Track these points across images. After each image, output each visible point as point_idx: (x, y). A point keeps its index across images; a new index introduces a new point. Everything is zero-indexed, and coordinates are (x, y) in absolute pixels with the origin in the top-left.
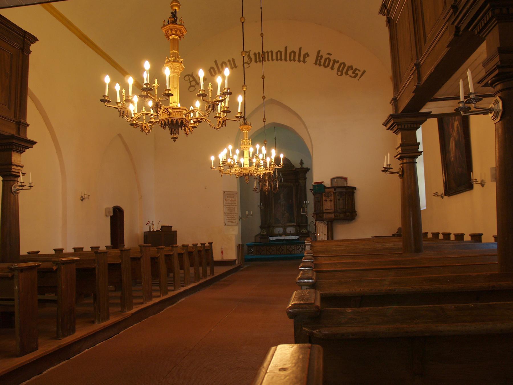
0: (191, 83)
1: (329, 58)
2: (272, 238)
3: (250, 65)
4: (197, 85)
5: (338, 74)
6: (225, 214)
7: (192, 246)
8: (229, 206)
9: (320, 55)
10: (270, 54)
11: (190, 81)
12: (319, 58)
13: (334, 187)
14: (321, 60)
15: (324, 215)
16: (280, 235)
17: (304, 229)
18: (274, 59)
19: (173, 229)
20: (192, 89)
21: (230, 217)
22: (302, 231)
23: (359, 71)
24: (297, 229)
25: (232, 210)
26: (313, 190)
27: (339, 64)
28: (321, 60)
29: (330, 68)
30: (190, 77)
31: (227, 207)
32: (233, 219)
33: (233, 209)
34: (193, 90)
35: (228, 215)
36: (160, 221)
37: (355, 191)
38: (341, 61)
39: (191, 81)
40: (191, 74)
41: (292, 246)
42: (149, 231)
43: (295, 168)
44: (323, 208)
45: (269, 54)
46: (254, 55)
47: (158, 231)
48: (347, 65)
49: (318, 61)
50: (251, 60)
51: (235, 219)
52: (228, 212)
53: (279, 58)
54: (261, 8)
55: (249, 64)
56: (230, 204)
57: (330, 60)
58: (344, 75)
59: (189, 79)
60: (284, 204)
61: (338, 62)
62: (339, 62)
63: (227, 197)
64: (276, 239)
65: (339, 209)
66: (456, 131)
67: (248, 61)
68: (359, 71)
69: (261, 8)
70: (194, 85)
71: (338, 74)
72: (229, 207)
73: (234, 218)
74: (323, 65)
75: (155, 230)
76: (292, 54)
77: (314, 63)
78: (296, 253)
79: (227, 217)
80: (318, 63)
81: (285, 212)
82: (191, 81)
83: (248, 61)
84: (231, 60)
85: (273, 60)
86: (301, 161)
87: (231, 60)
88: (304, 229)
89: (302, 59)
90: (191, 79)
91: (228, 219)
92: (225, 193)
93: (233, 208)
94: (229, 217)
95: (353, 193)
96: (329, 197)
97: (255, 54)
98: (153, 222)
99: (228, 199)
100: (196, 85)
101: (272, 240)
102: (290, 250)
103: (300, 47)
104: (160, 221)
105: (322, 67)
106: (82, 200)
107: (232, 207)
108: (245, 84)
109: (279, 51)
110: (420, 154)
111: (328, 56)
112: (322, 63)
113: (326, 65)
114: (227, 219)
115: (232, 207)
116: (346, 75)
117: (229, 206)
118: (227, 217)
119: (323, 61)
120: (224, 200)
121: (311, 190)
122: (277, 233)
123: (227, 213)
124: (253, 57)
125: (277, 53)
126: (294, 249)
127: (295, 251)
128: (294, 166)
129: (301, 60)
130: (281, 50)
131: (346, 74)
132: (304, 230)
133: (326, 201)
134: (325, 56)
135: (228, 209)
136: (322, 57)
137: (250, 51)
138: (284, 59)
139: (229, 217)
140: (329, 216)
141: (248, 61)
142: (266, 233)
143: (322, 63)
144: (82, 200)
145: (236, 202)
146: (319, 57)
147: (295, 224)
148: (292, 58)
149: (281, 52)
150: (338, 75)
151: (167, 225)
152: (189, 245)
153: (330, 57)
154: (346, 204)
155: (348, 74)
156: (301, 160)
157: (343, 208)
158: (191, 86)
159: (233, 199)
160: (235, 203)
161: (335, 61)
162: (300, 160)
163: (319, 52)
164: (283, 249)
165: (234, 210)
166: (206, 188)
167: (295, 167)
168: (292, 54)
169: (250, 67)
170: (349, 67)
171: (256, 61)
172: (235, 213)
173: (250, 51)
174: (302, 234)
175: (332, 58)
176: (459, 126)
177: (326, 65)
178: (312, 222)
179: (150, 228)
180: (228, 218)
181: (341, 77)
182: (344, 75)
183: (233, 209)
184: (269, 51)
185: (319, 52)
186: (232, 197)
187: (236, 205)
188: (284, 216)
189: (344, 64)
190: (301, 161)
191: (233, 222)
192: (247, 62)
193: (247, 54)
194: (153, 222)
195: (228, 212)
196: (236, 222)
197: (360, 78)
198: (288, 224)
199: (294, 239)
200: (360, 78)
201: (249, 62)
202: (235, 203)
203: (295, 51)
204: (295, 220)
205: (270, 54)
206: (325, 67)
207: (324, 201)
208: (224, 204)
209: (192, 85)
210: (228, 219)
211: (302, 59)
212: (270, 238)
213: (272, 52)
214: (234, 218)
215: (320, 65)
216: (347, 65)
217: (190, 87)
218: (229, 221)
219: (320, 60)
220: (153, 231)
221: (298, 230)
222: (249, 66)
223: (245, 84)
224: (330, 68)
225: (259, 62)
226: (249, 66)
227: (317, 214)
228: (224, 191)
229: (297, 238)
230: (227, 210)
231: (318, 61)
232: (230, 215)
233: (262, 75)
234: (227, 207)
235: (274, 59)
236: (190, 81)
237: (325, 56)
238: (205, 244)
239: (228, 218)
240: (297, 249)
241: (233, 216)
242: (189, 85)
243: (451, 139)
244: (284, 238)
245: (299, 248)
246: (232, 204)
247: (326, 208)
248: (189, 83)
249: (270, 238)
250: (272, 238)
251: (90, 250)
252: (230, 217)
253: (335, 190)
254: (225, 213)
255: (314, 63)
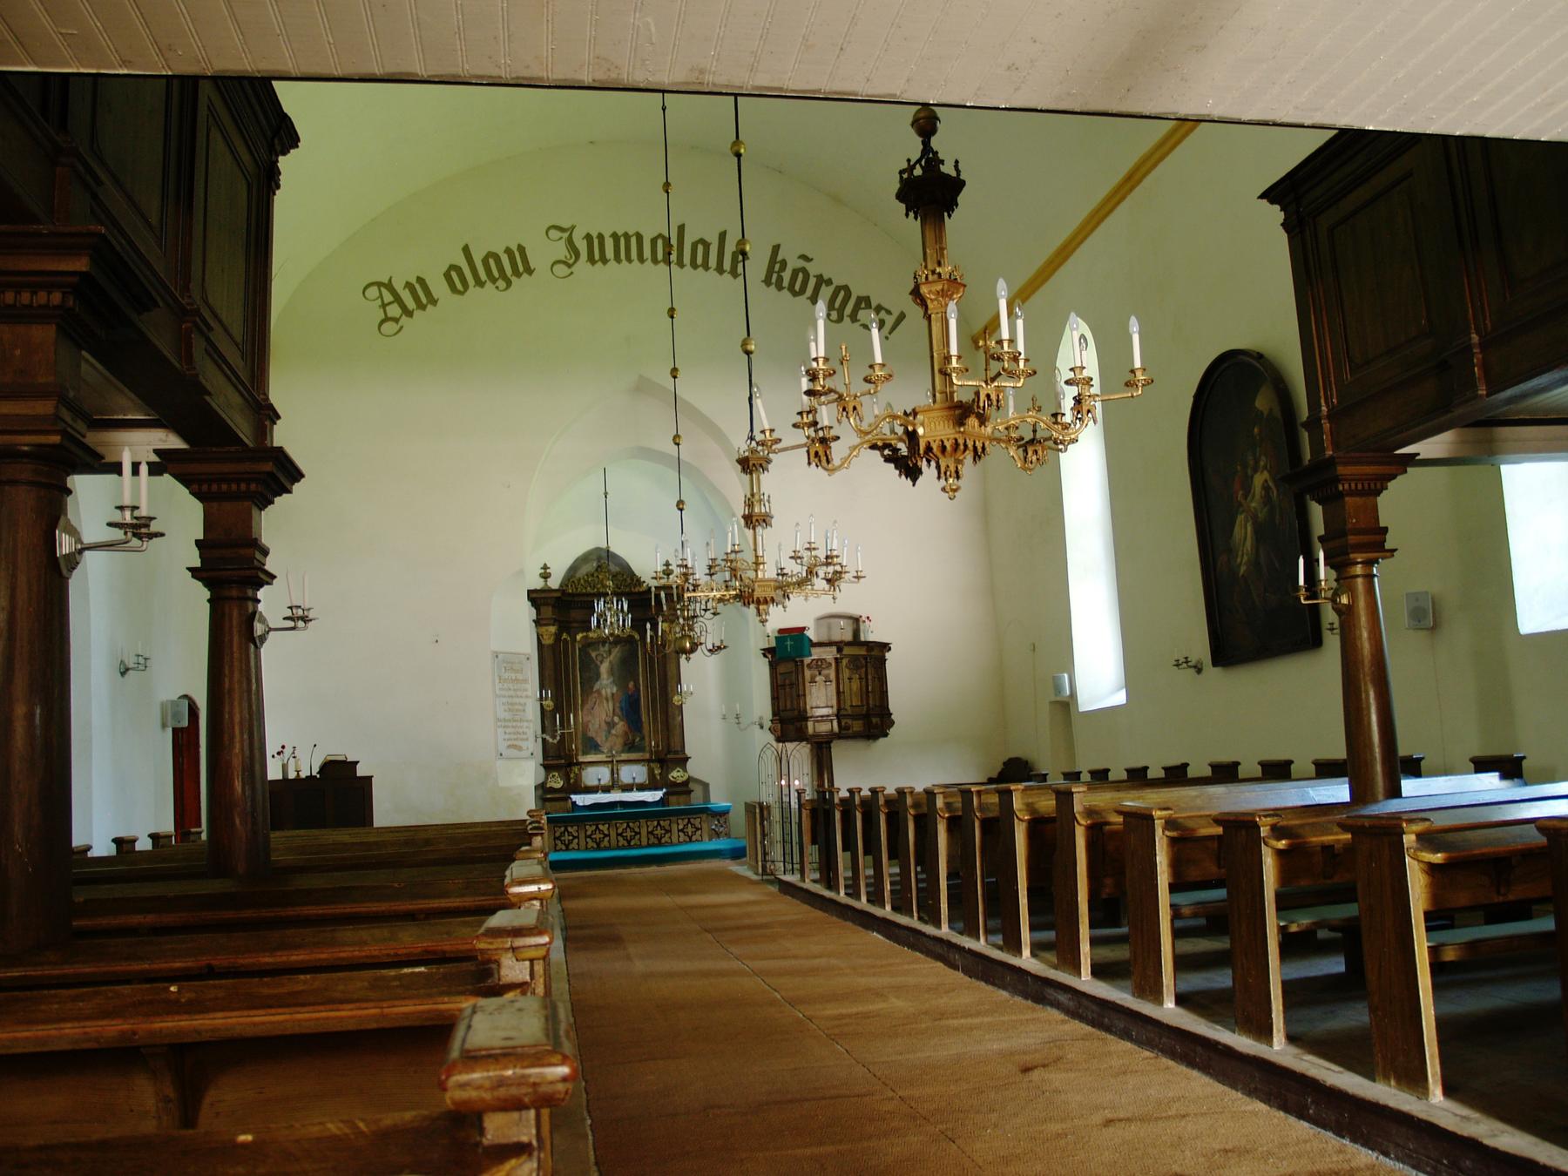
0: (388, 308)
1: (804, 270)
2: (581, 800)
3: (573, 269)
4: (407, 316)
5: (831, 318)
6: (499, 724)
7: (870, 794)
8: (509, 697)
9: (779, 258)
10: (633, 241)
11: (382, 301)
12: (777, 267)
13: (837, 642)
14: (783, 274)
15: (810, 724)
16: (606, 790)
17: (678, 771)
18: (647, 259)
19: (361, 771)
20: (389, 327)
21: (514, 733)
22: (673, 777)
23: (889, 312)
24: (653, 772)
25: (517, 710)
26: (769, 652)
27: (831, 289)
28: (783, 274)
29: (808, 298)
30: (382, 289)
31: (504, 700)
32: (522, 740)
33: (521, 708)
34: (395, 331)
35: (508, 727)
36: (315, 746)
37: (888, 655)
38: (836, 282)
39: (386, 302)
40: (386, 282)
41: (664, 820)
42: (281, 778)
43: (645, 585)
44: (805, 703)
45: (630, 241)
46: (585, 241)
47: (311, 778)
48: (856, 292)
49: (774, 272)
50: (577, 255)
51: (527, 739)
52: (507, 715)
53: (699, 261)
54: (664, 109)
55: (569, 266)
56: (512, 693)
57: (807, 275)
58: (847, 320)
59: (381, 296)
60: (613, 694)
61: (829, 282)
62: (832, 283)
63: (503, 670)
64: (593, 802)
65: (851, 706)
66: (1258, 497)
67: (569, 257)
68: (889, 312)
69: (664, 109)
70: (398, 317)
71: (831, 318)
72: (510, 700)
73: (525, 737)
74: (789, 289)
75: (303, 775)
76: (700, 248)
77: (762, 281)
78: (675, 839)
79: (505, 733)
80: (774, 280)
81: (616, 719)
82: (386, 302)
83: (566, 257)
84: (515, 249)
85: (629, 260)
86: (545, 567)
87: (515, 249)
88: (678, 769)
89: (727, 265)
90: (388, 297)
91: (508, 740)
92: (497, 656)
93: (520, 704)
94: (510, 733)
95: (882, 661)
96: (822, 672)
97: (589, 237)
98: (294, 748)
99: (506, 675)
100: (401, 315)
101: (581, 804)
102: (598, 836)
103: (723, 230)
104: (315, 746)
105: (786, 293)
106: (123, 674)
107: (517, 700)
108: (749, 335)
109: (660, 236)
110: (1388, 554)
111: (801, 263)
112: (786, 283)
113: (797, 288)
114: (504, 740)
115: (517, 700)
116: (853, 322)
117: (509, 697)
118: (505, 733)
119: (787, 276)
120: (497, 681)
121: (763, 650)
122: (595, 783)
123: (505, 720)
124: (582, 246)
125: (654, 241)
126: (640, 833)
127: (581, 843)
128: (642, 580)
129: (725, 268)
130: (708, 239)
131: (853, 317)
132: (679, 774)
133: (813, 681)
134: (793, 263)
135: (506, 707)
136: (784, 264)
137: (573, 227)
138: (729, 270)
139: (510, 733)
140: (824, 728)
141: (566, 257)
142: (562, 783)
143: (786, 283)
144: (123, 674)
145: (528, 686)
146: (776, 263)
147: (647, 756)
148: (699, 261)
149: (707, 245)
150: (832, 321)
151: (343, 758)
152: (884, 788)
153: (808, 266)
154: (868, 692)
155: (859, 320)
156: (667, 561)
157: (859, 704)
158: (386, 319)
159: (520, 676)
160: (526, 690)
161: (821, 281)
162: (542, 566)
163: (776, 249)
164: (637, 830)
165: (524, 710)
166: (437, 641)
167: (644, 582)
168: (700, 248)
169: (572, 276)
170: (860, 300)
171: (592, 260)
172: (527, 721)
173: (573, 227)
174: (675, 784)
175: (813, 269)
176: (1271, 484)
177: (797, 288)
178: (769, 746)
179: (285, 768)
180: (507, 737)
181: (837, 325)
182: (847, 320)
183: (521, 708)
184: (630, 233)
185: (776, 249)
186: (517, 671)
187: (527, 697)
188: (613, 732)
189: (846, 288)
190: (545, 567)
191: (520, 748)
192: (564, 259)
193: (566, 235)
194: (294, 748)
195: (507, 715)
196: (528, 748)
197: (890, 333)
198: (624, 756)
199: (650, 800)
200: (890, 333)
201: (571, 262)
202: (526, 690)
203: (709, 241)
204: (647, 744)
205: (633, 241)
206: (795, 294)
207: (807, 684)
208: (497, 692)
209: (389, 315)
210: (508, 740)
211: (727, 265)
212: (574, 797)
213: (639, 237)
214: (525, 737)
215: (780, 287)
216: (856, 292)
217: (382, 322)
218: (509, 747)
219: (778, 272)
220: (298, 780)
221: (656, 772)
222: (569, 271)
223: (749, 335)
224: (808, 298)
225: (600, 264)
226: (572, 273)
227: (782, 721)
228: (496, 652)
229: (657, 798)
230: (505, 711)
231: (775, 276)
232: (513, 727)
233: (670, 306)
234: (504, 700)
235: (647, 259)
236: (382, 301)
237: (793, 263)
238: (133, 841)
239: (507, 737)
240: (679, 831)
241: (521, 730)
242: (383, 316)
243: (1241, 518)
244: (618, 799)
245: (563, 834)
246: (519, 693)
247: (814, 705)
248: (382, 310)
249: (574, 800)
250: (581, 800)
251: (894, 792)
252: (514, 733)
253: (839, 650)
254: (499, 720)
255: (762, 281)
